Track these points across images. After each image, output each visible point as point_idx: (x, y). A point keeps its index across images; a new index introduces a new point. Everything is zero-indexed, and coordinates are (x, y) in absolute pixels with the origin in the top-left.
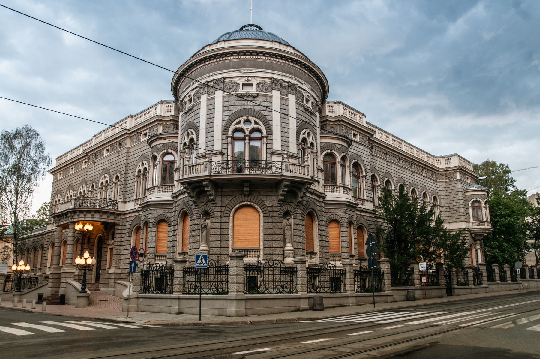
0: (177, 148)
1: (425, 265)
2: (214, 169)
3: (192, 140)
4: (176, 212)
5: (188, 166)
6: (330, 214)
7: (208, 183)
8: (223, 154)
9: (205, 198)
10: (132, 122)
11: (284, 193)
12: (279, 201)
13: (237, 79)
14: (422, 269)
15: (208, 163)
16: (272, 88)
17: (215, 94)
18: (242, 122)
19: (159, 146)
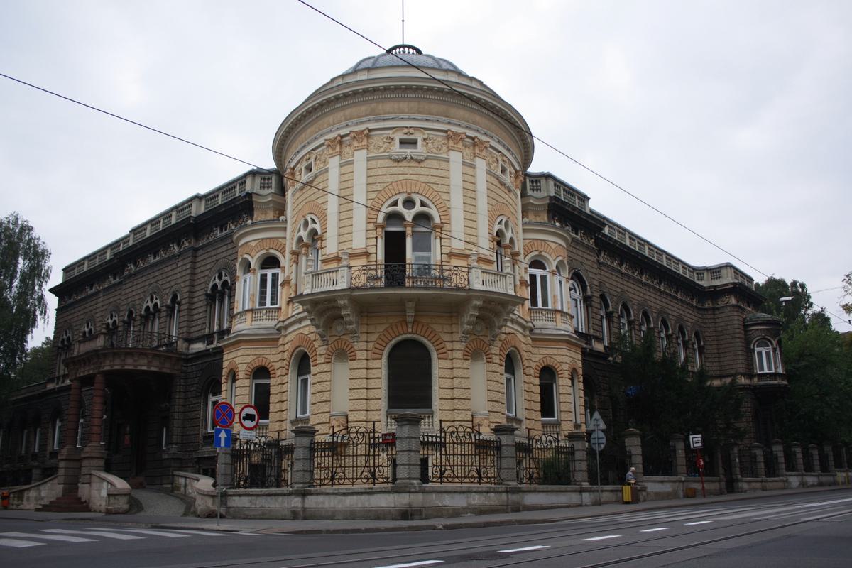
0: (284, 247)
1: (700, 439)
2: (357, 279)
3: (314, 232)
4: (286, 353)
5: (310, 275)
6: (541, 356)
7: (346, 302)
8: (367, 255)
9: (339, 328)
10: (200, 206)
11: (472, 319)
12: (463, 333)
13: (391, 132)
14: (696, 445)
15: (346, 269)
16: (448, 147)
17: (353, 155)
18: (400, 203)
19: (253, 244)
